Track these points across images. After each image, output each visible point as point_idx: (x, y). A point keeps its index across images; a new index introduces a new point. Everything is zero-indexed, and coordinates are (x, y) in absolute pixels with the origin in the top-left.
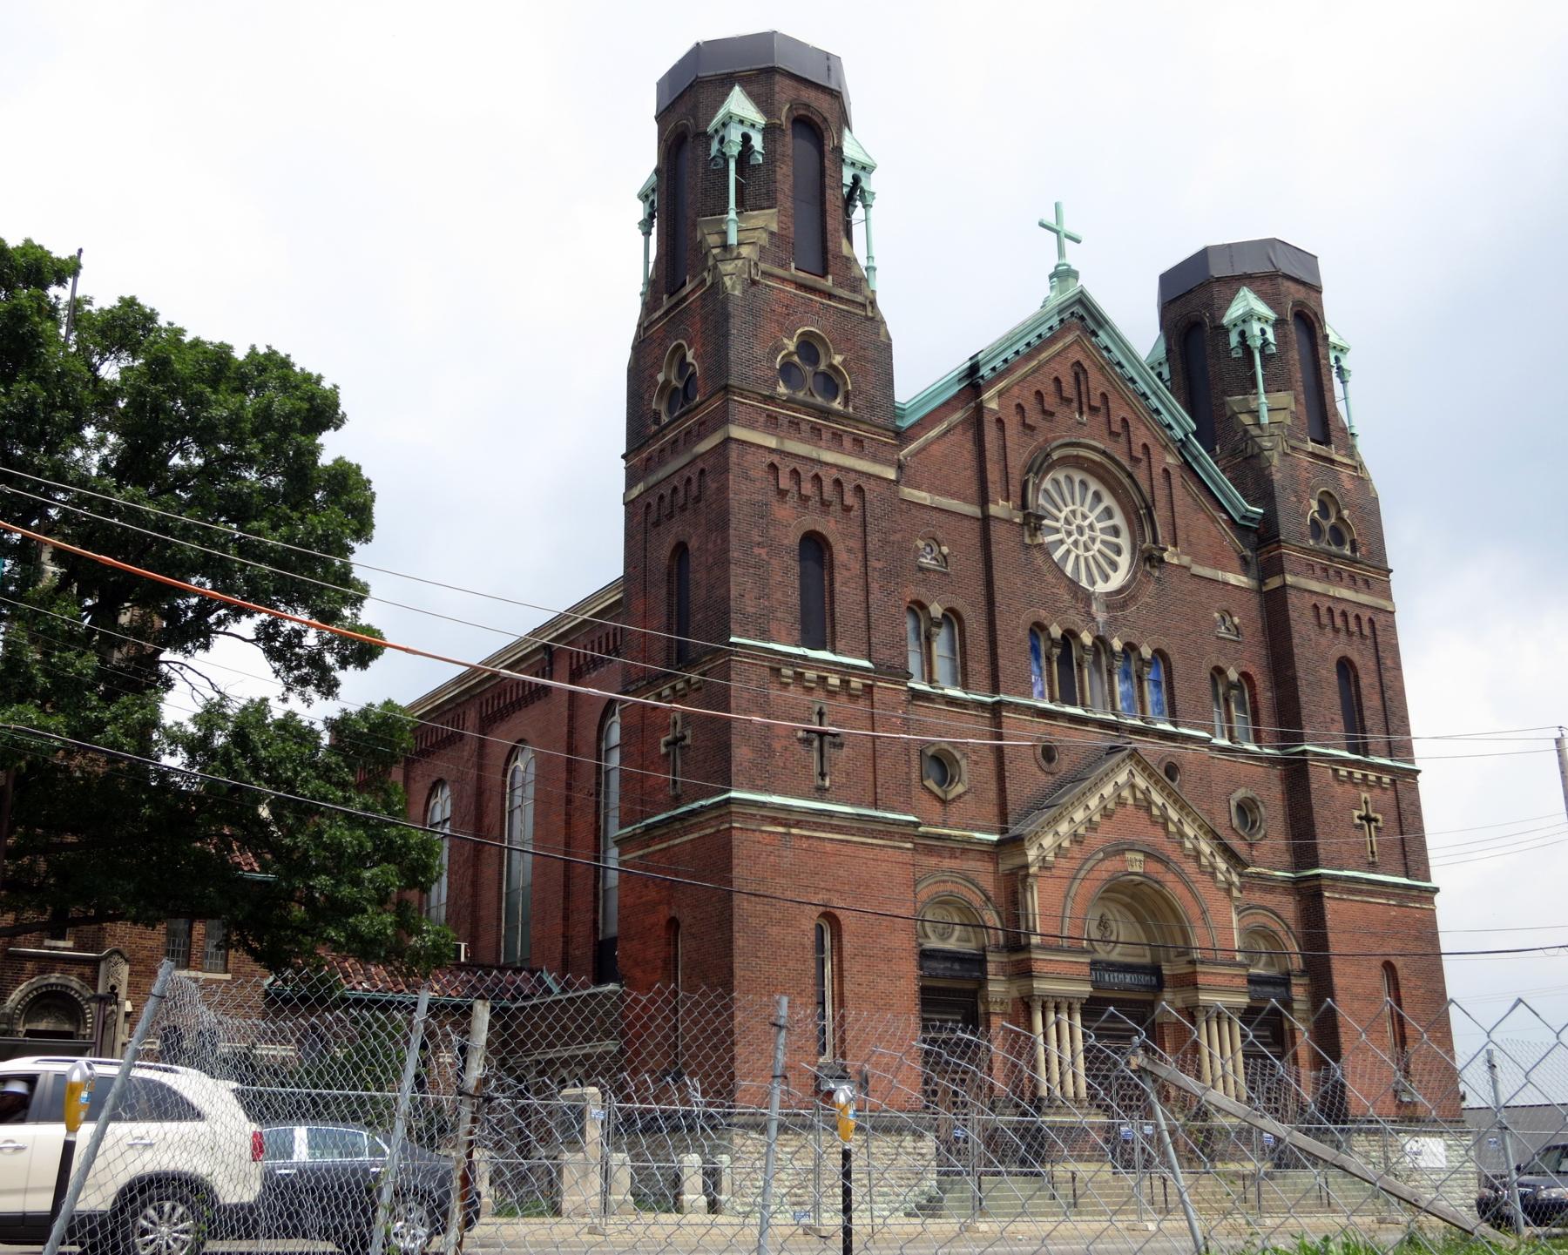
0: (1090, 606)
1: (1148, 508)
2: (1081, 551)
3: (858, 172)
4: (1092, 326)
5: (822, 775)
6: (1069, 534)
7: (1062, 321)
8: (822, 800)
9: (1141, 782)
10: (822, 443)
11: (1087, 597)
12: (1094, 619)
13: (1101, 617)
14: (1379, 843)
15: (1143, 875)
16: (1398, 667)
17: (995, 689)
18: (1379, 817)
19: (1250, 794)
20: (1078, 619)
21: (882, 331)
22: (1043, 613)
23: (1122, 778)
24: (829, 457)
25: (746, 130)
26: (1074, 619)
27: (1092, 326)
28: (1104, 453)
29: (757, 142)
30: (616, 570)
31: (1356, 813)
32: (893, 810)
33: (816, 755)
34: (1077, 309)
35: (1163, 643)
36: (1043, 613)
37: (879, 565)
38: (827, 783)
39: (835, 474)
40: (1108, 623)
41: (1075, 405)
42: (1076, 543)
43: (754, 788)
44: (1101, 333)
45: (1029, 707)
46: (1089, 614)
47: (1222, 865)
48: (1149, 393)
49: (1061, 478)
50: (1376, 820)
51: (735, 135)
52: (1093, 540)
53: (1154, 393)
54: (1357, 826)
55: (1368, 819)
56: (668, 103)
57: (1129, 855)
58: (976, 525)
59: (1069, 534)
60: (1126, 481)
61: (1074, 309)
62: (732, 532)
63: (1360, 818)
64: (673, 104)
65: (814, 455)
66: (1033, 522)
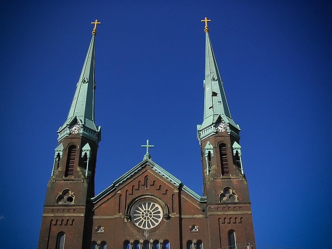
6: (145, 218)
10: (65, 212)
11: (143, 231)
22: (128, 238)
24: (66, 215)
26: (138, 237)
39: (68, 218)
40: (149, 236)
48: (168, 177)
52: (151, 213)
65: (63, 215)
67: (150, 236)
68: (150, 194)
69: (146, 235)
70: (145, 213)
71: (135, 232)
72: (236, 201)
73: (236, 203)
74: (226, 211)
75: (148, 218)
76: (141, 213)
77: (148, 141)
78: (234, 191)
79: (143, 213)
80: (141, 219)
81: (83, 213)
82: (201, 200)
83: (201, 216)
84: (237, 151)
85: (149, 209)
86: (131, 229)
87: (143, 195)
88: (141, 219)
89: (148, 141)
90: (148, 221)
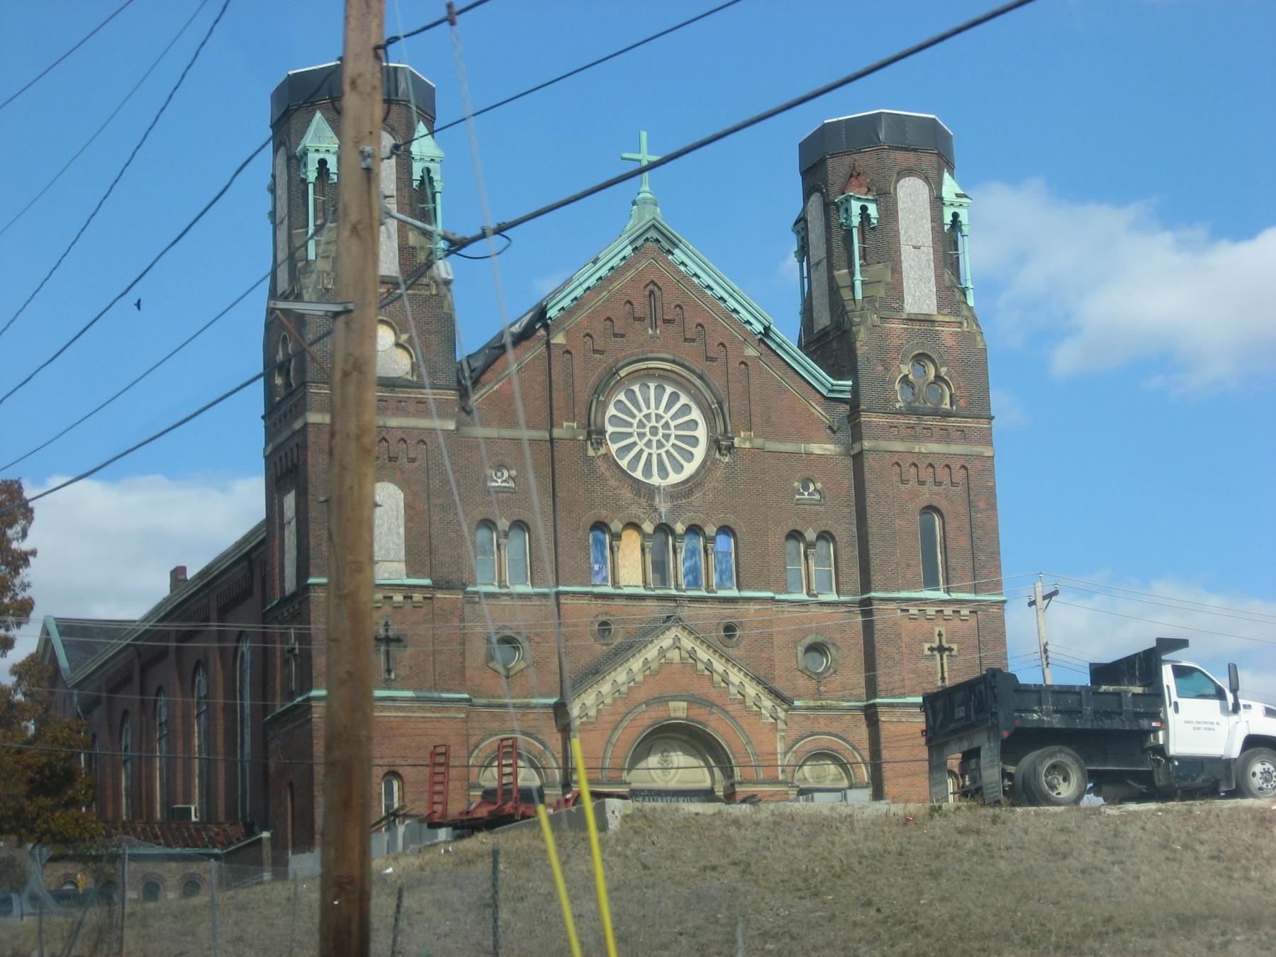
0: (653, 499)
1: (720, 404)
2: (654, 451)
3: (427, 165)
4: (667, 246)
5: (389, 671)
6: (641, 435)
7: (635, 249)
8: (389, 688)
9: (687, 643)
10: (389, 413)
11: (651, 491)
12: (656, 510)
13: (663, 507)
14: (951, 670)
15: (687, 719)
16: (993, 506)
17: (557, 584)
18: (955, 646)
19: (820, 639)
20: (640, 512)
21: (446, 304)
22: (604, 513)
23: (666, 641)
25: (321, 156)
26: (635, 511)
27: (667, 246)
28: (674, 362)
29: (332, 166)
30: (264, 516)
31: (927, 646)
32: (449, 691)
33: (383, 657)
34: (653, 234)
35: (730, 520)
36: (604, 513)
37: (439, 502)
38: (393, 676)
39: (400, 435)
41: (648, 321)
42: (649, 444)
43: (886, 590)
44: (676, 251)
45: (586, 594)
46: (652, 506)
47: (767, 703)
48: (726, 296)
49: (622, 397)
50: (950, 650)
51: (313, 159)
52: (667, 437)
53: (731, 295)
54: (926, 657)
55: (941, 649)
56: (276, 118)
57: (671, 704)
58: (548, 444)
59: (641, 435)
60: (698, 382)
61: (648, 235)
62: (310, 497)
63: (931, 649)
64: (279, 119)
66: (596, 434)
67: (676, 511)
68: (667, 356)
69: (663, 507)
70: (660, 436)
71: (626, 494)
72: (946, 405)
73: (947, 414)
74: (916, 438)
75: (644, 434)
76: (645, 411)
77: (644, 135)
78: (943, 370)
79: (648, 416)
80: (640, 410)
81: (451, 418)
82: (831, 391)
83: (829, 448)
84: (955, 215)
85: (635, 438)
86: (612, 482)
87: (642, 360)
88: (640, 410)
89: (644, 135)
90: (659, 455)
